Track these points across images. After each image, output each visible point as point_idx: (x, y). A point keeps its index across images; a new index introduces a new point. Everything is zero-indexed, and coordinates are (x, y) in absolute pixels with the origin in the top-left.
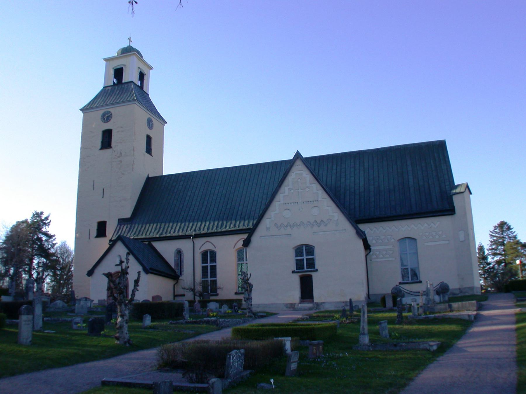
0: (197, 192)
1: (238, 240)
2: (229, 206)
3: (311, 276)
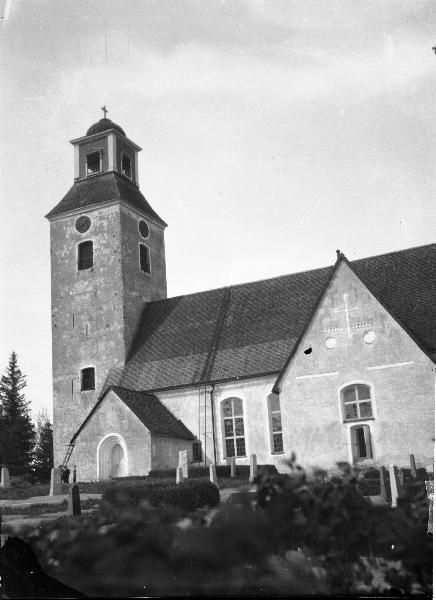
1: (264, 389)
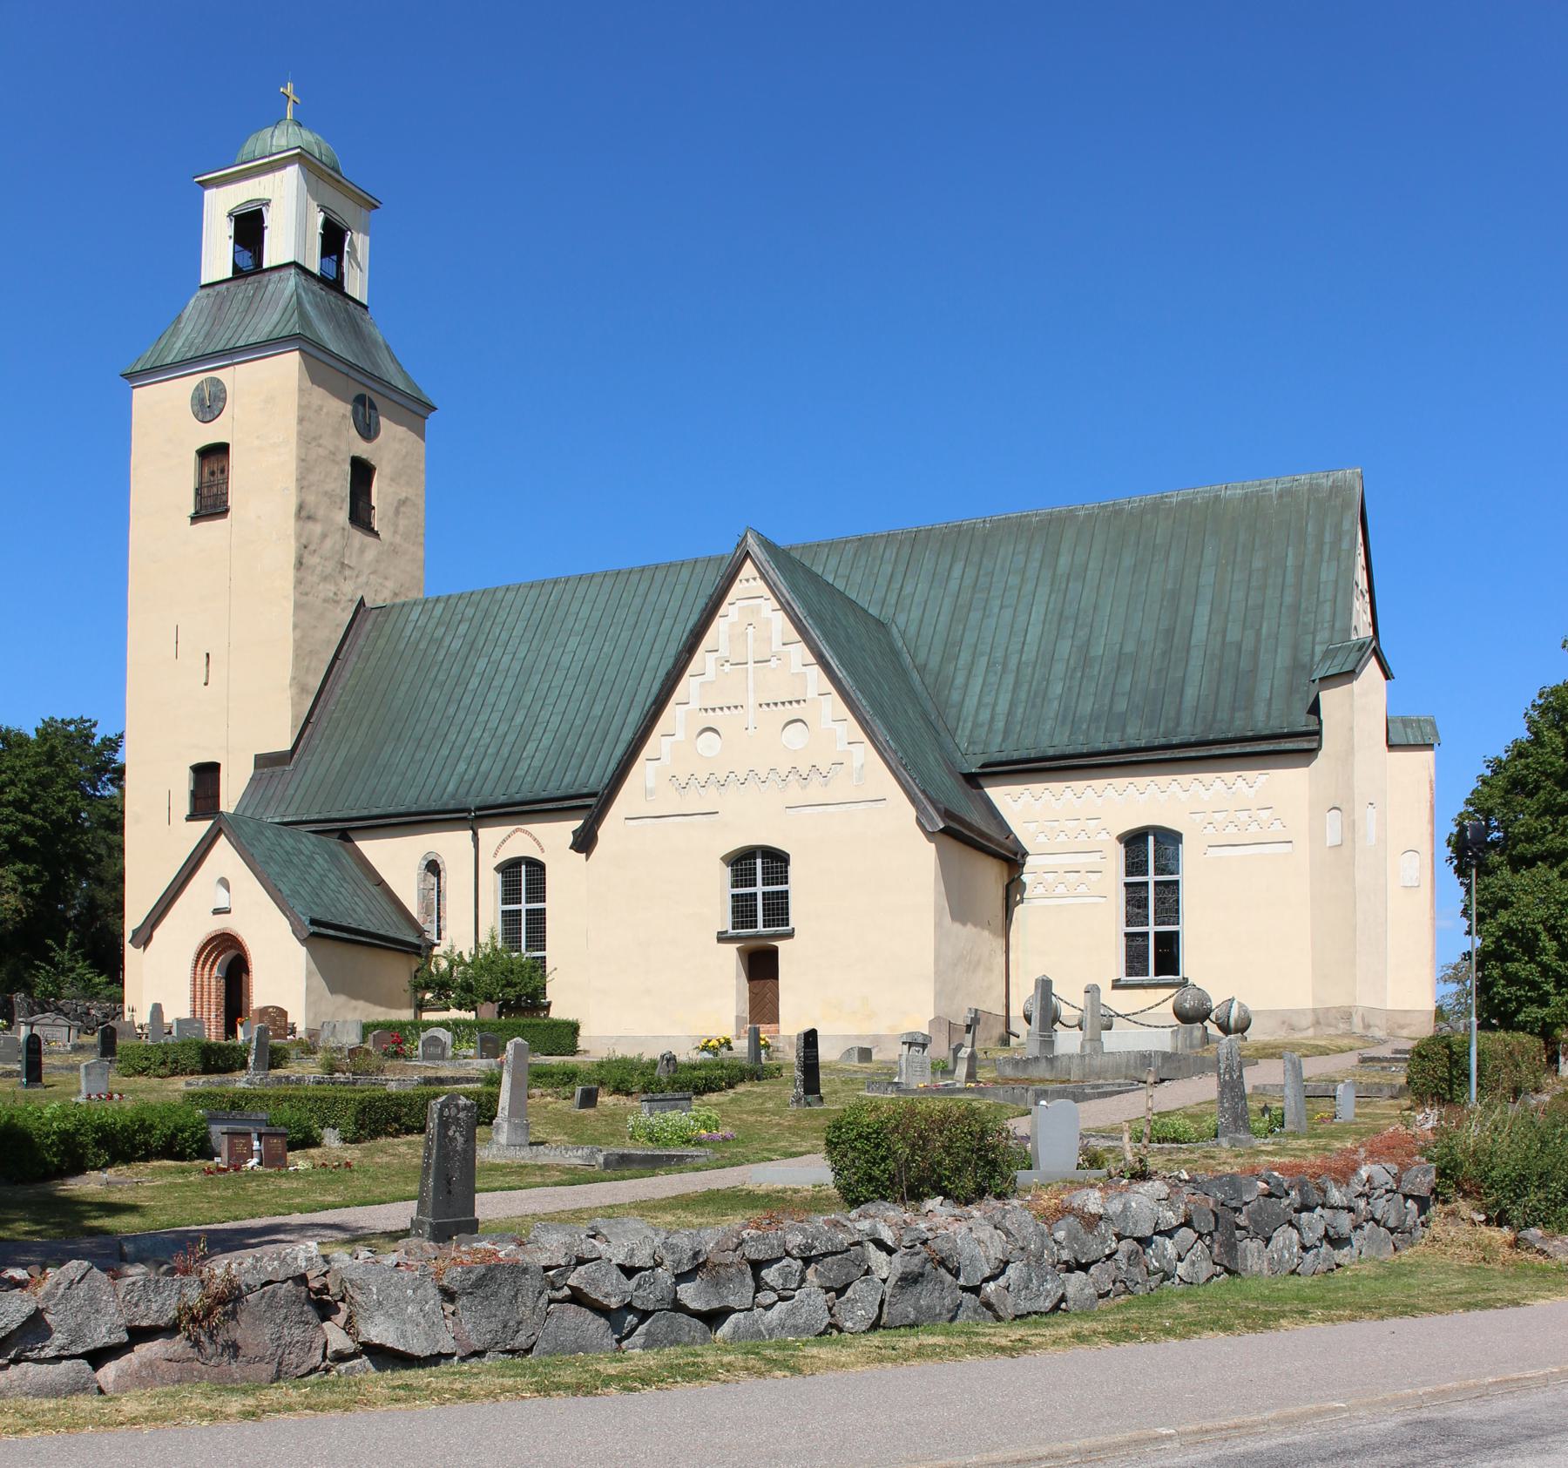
0: (507, 659)
2: (597, 710)
3: (774, 952)
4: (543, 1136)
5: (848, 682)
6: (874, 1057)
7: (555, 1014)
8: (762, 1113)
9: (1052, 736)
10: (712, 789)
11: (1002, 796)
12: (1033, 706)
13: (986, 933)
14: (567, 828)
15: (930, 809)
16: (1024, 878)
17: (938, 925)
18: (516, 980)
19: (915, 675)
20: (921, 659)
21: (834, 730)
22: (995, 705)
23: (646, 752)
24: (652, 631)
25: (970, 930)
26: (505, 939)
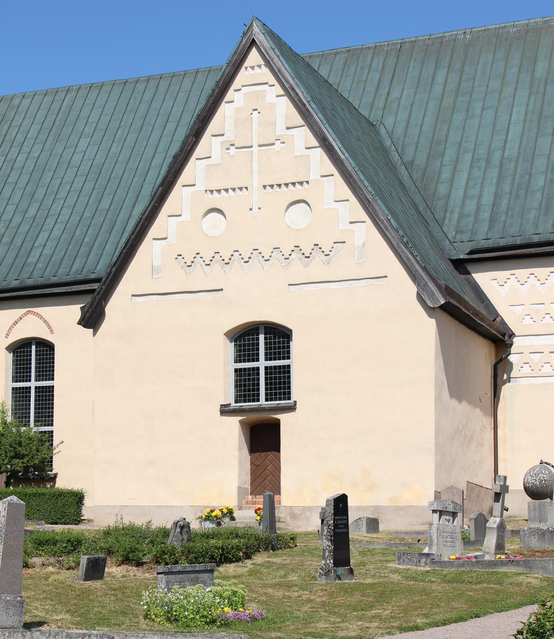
2: (105, 204)
3: (276, 426)
4: (40, 614)
5: (350, 164)
6: (381, 527)
7: (60, 484)
8: (289, 586)
9: (536, 225)
10: (217, 267)
11: (487, 280)
12: (517, 197)
13: (478, 411)
14: (73, 311)
15: (431, 285)
16: (511, 358)
17: (438, 398)
18: (23, 451)
19: (403, 170)
20: (408, 157)
21: (335, 208)
22: (480, 196)
23: (154, 231)
24: (156, 133)
25: (465, 405)
26: (14, 414)
